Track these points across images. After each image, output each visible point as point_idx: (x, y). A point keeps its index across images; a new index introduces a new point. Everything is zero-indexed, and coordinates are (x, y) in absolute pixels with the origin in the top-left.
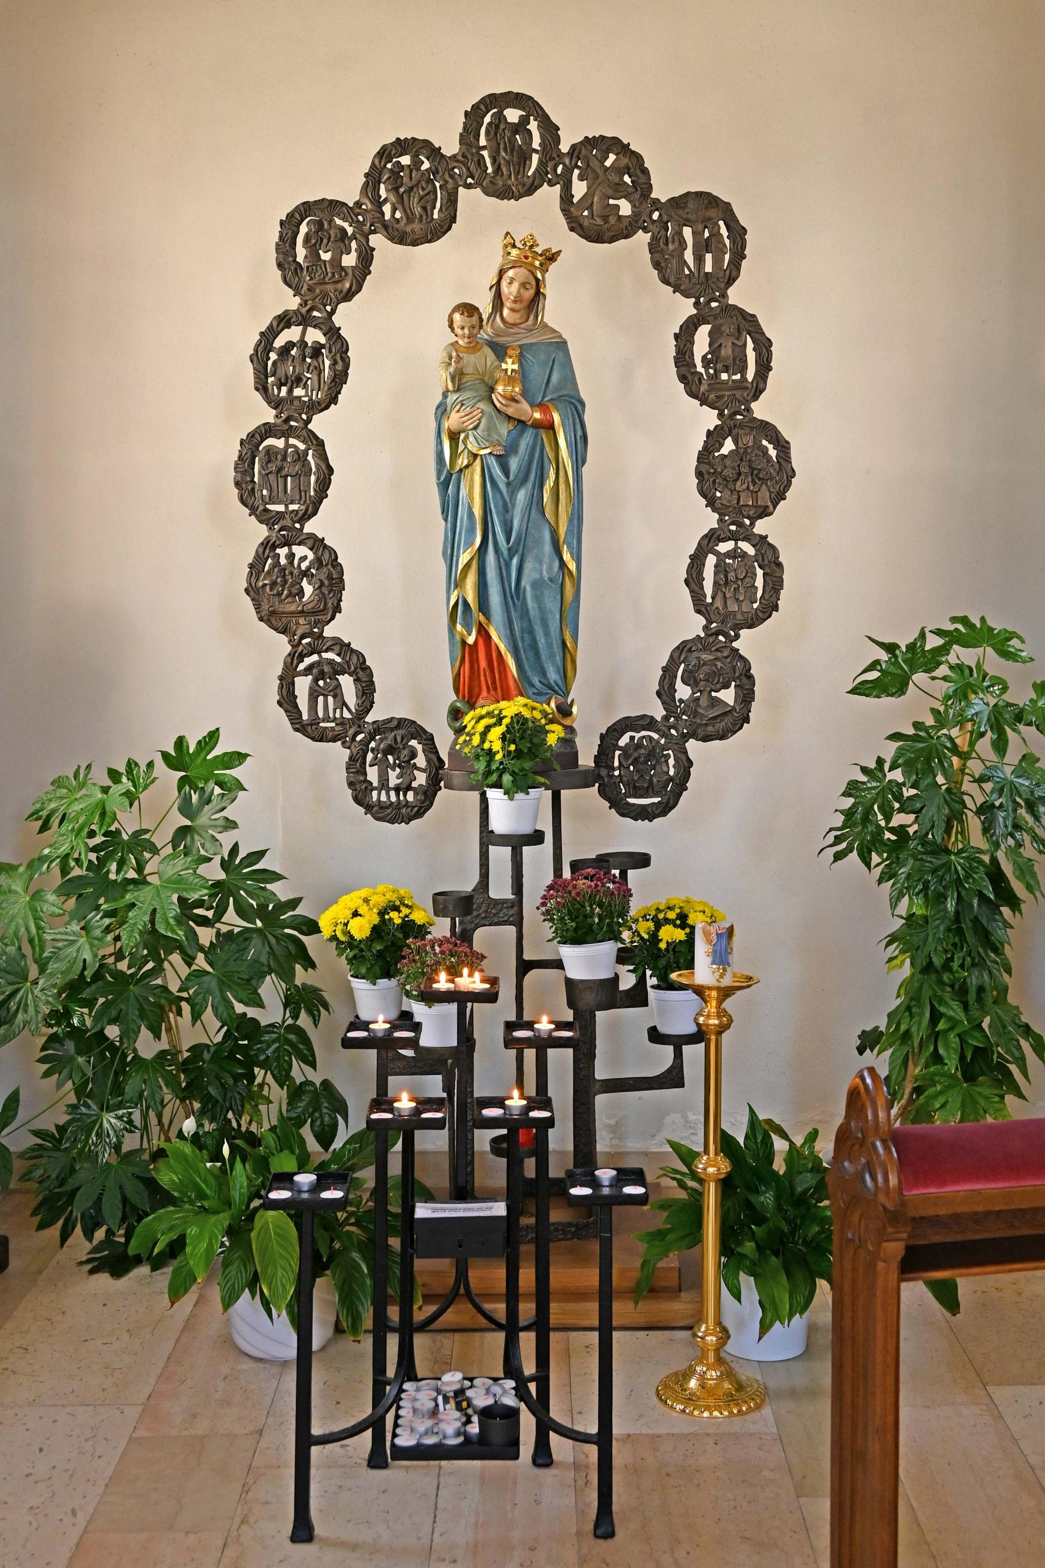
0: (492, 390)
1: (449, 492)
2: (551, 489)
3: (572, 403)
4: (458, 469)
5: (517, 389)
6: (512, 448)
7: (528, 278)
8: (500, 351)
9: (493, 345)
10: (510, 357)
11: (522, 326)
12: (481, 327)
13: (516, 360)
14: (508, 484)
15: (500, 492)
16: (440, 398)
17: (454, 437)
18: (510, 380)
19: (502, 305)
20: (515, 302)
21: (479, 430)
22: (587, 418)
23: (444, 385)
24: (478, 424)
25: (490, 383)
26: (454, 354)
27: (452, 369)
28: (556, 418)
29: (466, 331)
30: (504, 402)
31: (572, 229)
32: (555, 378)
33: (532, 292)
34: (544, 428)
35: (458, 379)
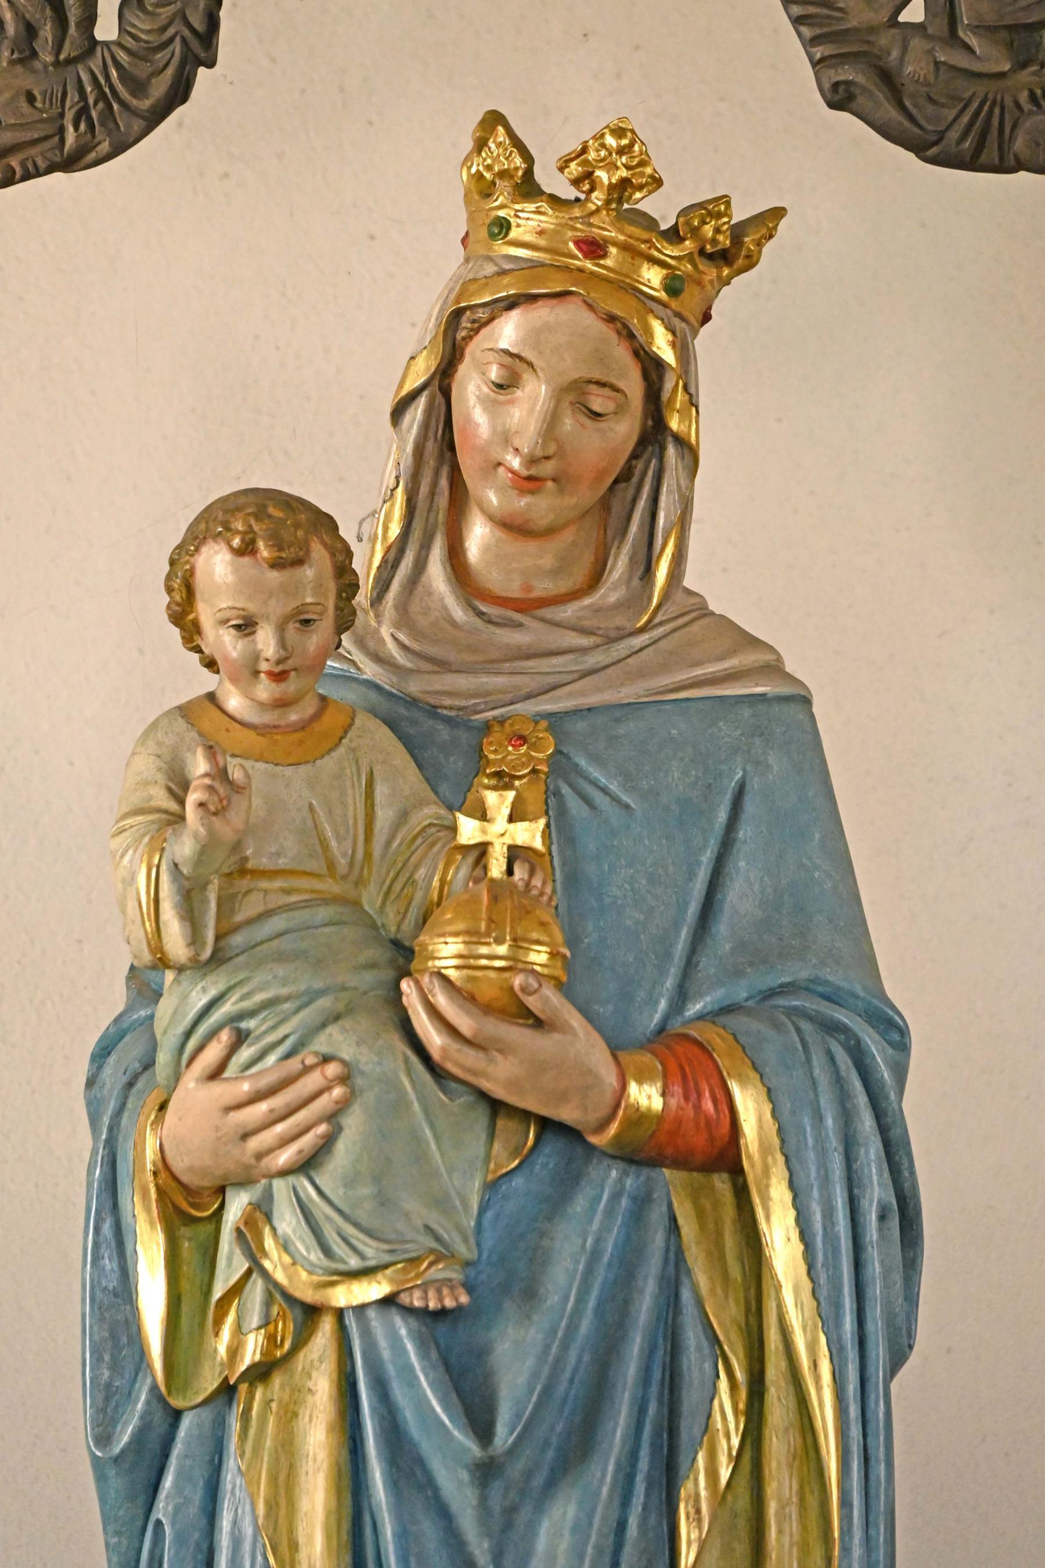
0: (404, 957)
1: (162, 1510)
2: (721, 1498)
3: (832, 1028)
4: (210, 1384)
5: (539, 956)
6: (508, 1276)
7: (601, 359)
8: (447, 746)
9: (409, 719)
10: (503, 780)
11: (568, 612)
12: (345, 621)
13: (535, 798)
14: (486, 1472)
15: (444, 1514)
16: (116, 997)
17: (189, 1209)
18: (503, 903)
19: (459, 497)
20: (529, 483)
21: (330, 1175)
22: (916, 1107)
23: (139, 934)
24: (327, 1144)
25: (390, 922)
26: (199, 765)
27: (184, 848)
28: (750, 1107)
29: (266, 641)
30: (465, 1023)
31: (840, 98)
32: (740, 897)
33: (625, 430)
34: (681, 1162)
35: (223, 903)
